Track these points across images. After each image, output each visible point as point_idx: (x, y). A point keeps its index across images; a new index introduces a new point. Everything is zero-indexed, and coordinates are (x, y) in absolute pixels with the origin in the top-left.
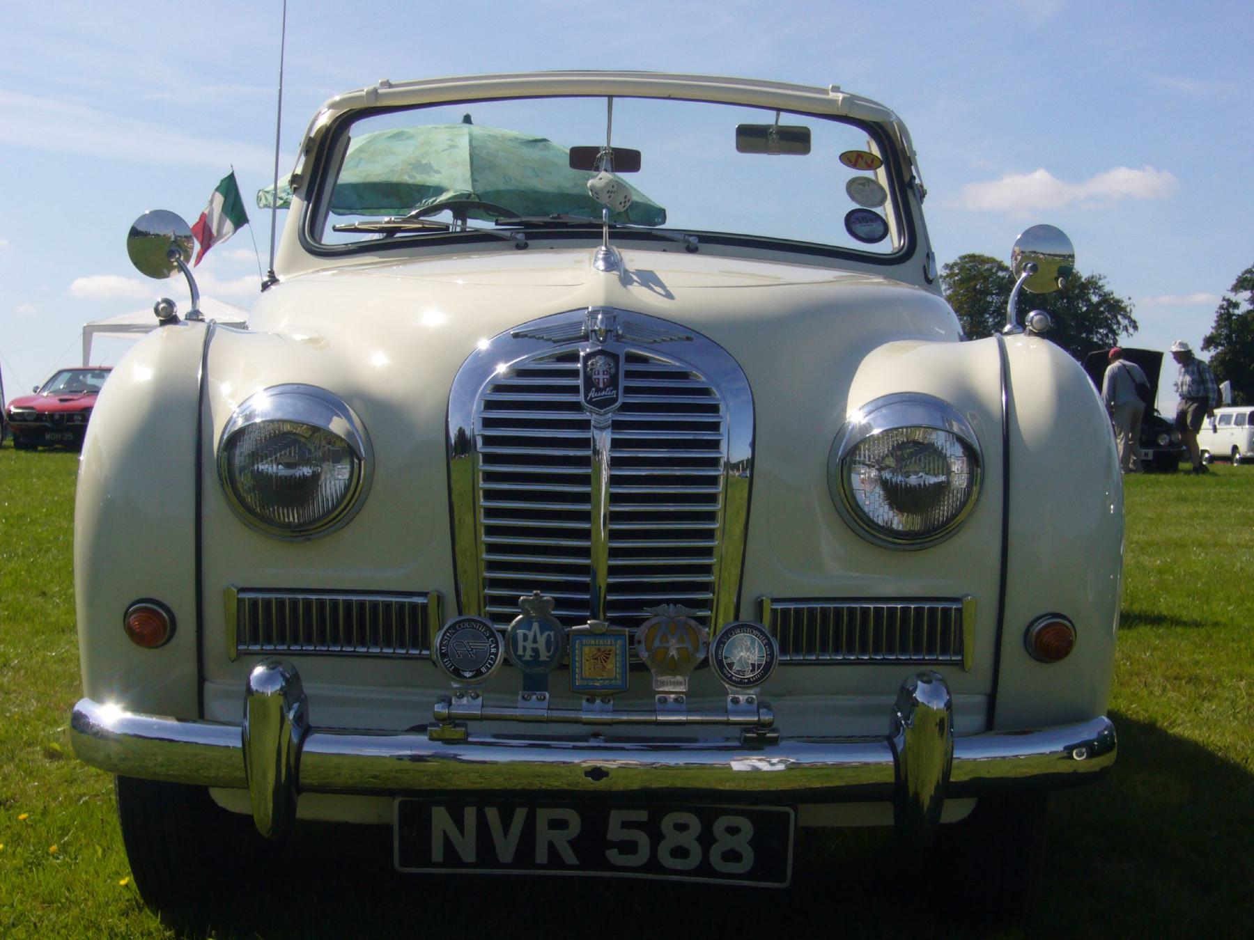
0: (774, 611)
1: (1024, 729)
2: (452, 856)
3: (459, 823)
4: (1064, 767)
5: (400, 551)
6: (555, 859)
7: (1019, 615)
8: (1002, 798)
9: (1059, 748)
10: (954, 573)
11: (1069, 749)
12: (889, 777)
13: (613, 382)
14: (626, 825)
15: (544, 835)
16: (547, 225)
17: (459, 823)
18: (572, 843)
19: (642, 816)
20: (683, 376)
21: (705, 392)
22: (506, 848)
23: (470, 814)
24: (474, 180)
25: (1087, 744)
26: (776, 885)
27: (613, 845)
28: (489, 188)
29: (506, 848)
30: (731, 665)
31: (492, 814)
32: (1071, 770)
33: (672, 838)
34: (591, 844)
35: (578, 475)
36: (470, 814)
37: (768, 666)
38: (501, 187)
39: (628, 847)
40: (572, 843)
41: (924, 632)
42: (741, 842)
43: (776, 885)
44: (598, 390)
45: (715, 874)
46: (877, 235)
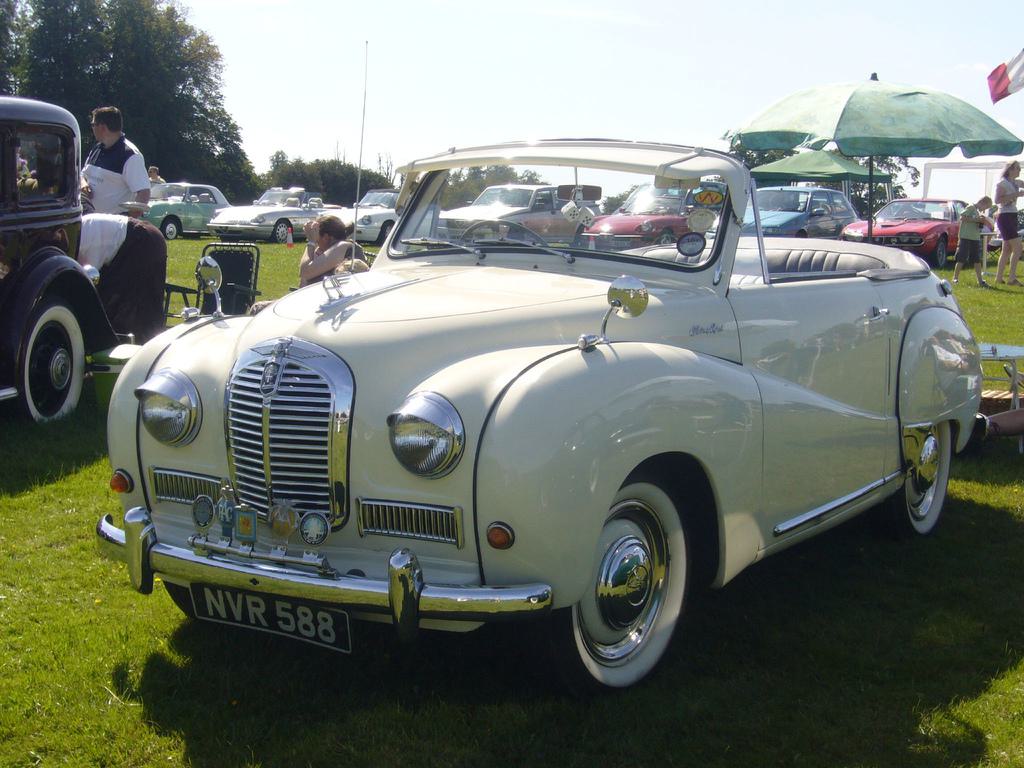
1: (502, 584)
2: (217, 614)
3: (216, 597)
4: (526, 607)
7: (486, 520)
8: (497, 625)
10: (447, 493)
13: (273, 381)
14: (284, 609)
15: (251, 610)
16: (499, 244)
17: (216, 597)
18: (264, 615)
19: (288, 606)
20: (316, 377)
21: (325, 386)
23: (240, 596)
25: (538, 596)
26: (344, 651)
27: (280, 619)
28: (848, 136)
29: (238, 614)
30: (307, 534)
31: (228, 594)
32: (529, 609)
33: (303, 621)
34: (271, 615)
35: (248, 434)
36: (240, 596)
37: (325, 536)
38: (859, 134)
39: (286, 621)
40: (264, 615)
41: (438, 524)
43: (344, 651)
44: (267, 384)
45: (300, 635)
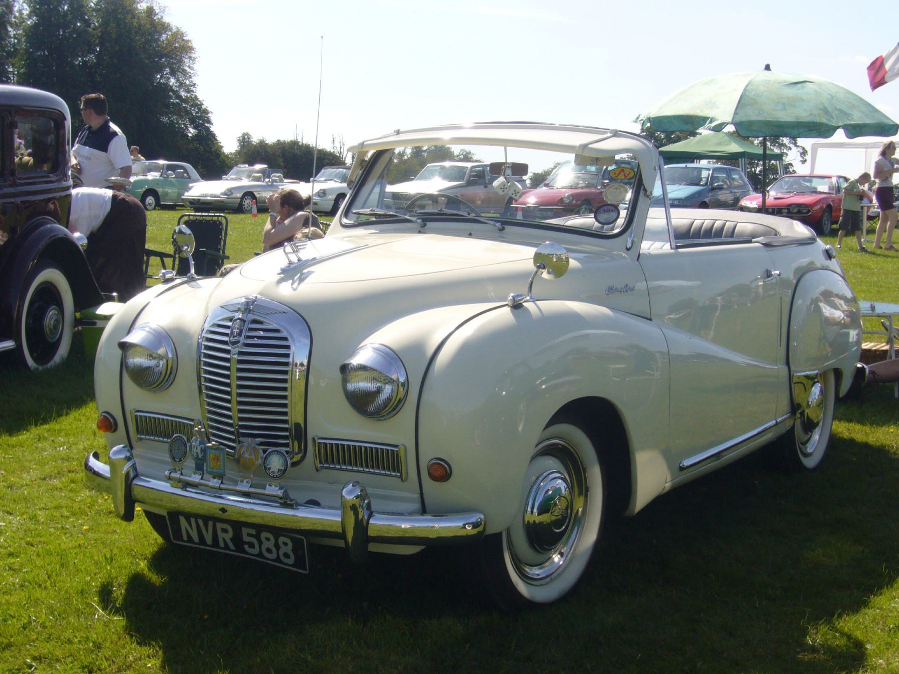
0: (320, 443)
1: (441, 512)
4: (462, 533)
5: (182, 402)
6: (226, 547)
7: (426, 459)
9: (461, 524)
11: (465, 525)
12: (340, 530)
13: (240, 334)
14: (249, 535)
15: (221, 535)
17: (206, 526)
19: (253, 532)
20: (277, 331)
21: (285, 339)
22: (209, 539)
24: (736, 113)
28: (744, 119)
30: (270, 469)
31: (201, 522)
34: (237, 540)
36: (210, 523)
37: (285, 470)
41: (385, 460)
42: (289, 549)
45: (281, 562)
46: (612, 220)
